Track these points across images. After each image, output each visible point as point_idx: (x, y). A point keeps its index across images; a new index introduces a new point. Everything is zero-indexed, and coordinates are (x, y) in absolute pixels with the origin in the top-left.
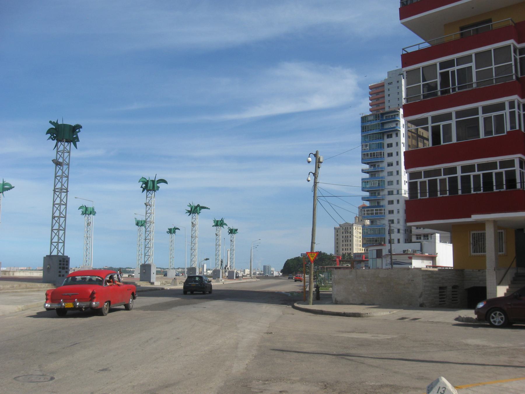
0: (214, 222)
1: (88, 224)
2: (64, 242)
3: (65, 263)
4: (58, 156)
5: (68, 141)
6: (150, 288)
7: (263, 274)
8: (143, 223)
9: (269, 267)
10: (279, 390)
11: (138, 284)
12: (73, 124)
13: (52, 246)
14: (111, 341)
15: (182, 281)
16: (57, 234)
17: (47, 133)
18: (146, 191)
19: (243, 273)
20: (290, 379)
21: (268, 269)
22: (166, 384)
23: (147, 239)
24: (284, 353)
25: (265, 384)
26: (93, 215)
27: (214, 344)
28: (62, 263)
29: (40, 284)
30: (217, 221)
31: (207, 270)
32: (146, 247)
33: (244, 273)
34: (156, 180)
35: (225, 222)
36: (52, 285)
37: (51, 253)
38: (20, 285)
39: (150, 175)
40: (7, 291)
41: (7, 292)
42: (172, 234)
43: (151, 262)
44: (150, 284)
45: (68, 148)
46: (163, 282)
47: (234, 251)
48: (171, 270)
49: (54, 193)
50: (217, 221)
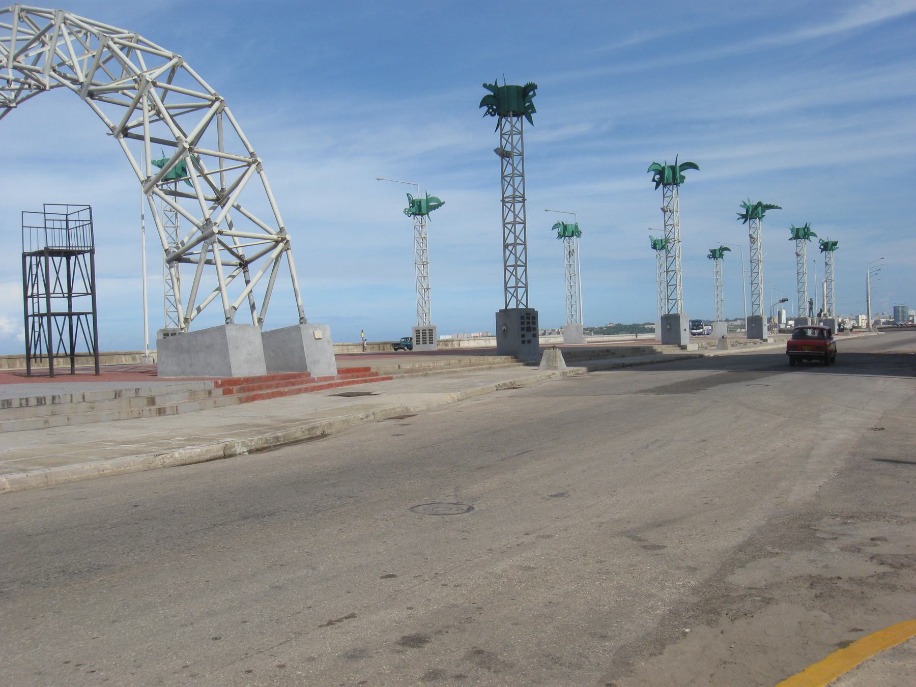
0: (792, 231)
1: (571, 253)
2: (526, 286)
3: (531, 320)
4: (504, 142)
5: (517, 114)
6: (677, 357)
7: (894, 323)
8: (664, 243)
9: (904, 310)
10: (872, 536)
11: (659, 350)
12: (522, 84)
13: (508, 293)
14: (585, 447)
15: (737, 341)
16: (514, 273)
17: (481, 106)
18: (661, 185)
19: (855, 322)
20: (897, 516)
21: (903, 313)
22: (660, 520)
23: (669, 270)
24: (899, 466)
25: (845, 523)
26: (577, 237)
27: (765, 451)
28: (525, 320)
29: (492, 357)
30: (798, 230)
31: (787, 320)
32: (669, 284)
33: (858, 322)
34: (679, 164)
35: (811, 231)
36: (512, 358)
37: (507, 305)
38: (460, 361)
39: (667, 159)
40: (439, 371)
41: (439, 373)
42: (717, 258)
43: (679, 310)
44: (680, 348)
45: (518, 125)
46: (703, 343)
47: (833, 283)
48: (719, 322)
49: (504, 205)
50: (797, 229)
